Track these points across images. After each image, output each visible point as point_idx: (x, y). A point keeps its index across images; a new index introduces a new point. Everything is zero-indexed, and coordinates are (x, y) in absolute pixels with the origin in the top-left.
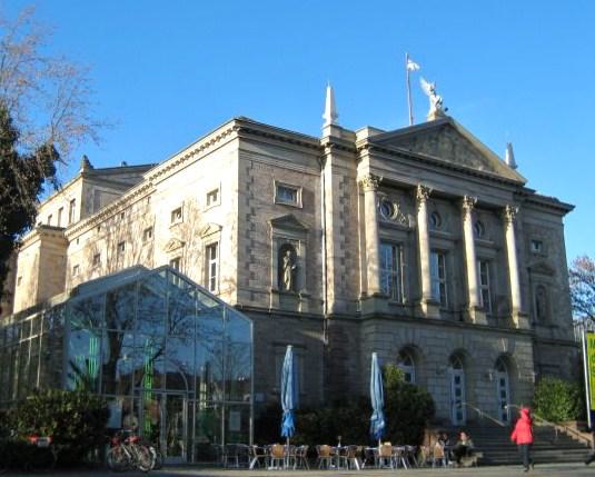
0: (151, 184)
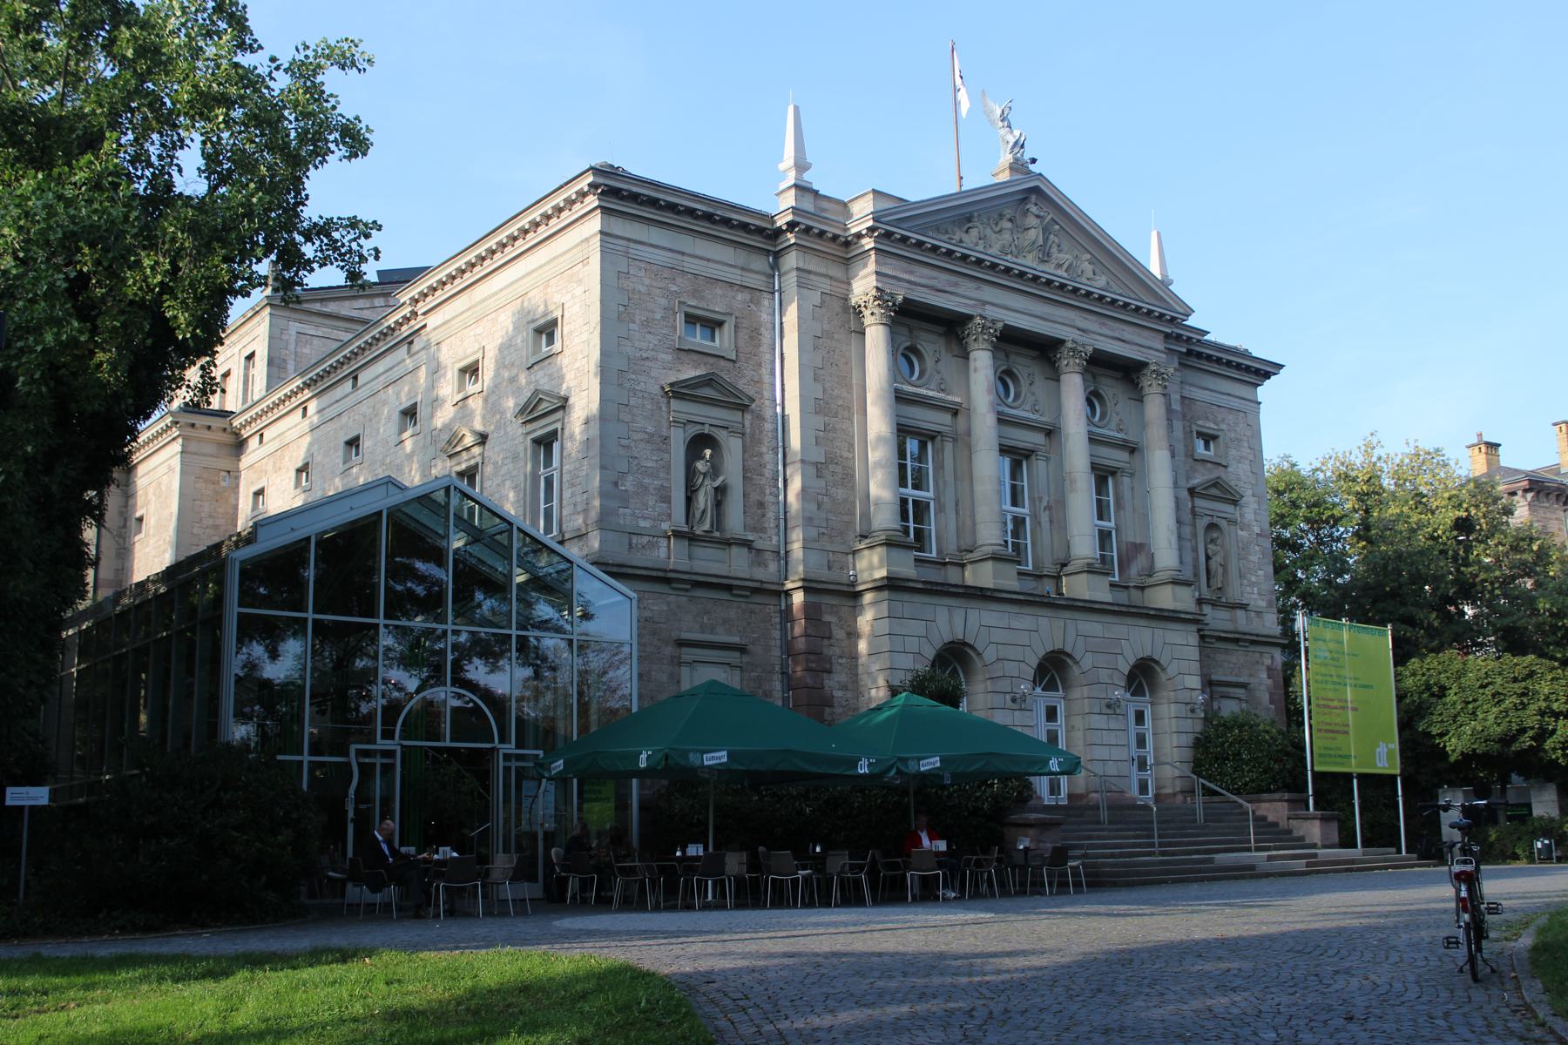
0: (415, 314)
